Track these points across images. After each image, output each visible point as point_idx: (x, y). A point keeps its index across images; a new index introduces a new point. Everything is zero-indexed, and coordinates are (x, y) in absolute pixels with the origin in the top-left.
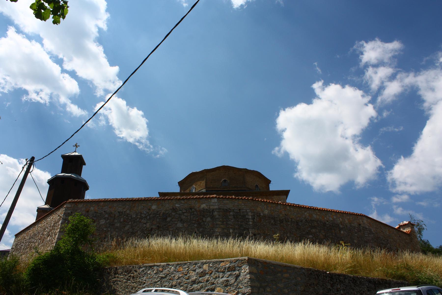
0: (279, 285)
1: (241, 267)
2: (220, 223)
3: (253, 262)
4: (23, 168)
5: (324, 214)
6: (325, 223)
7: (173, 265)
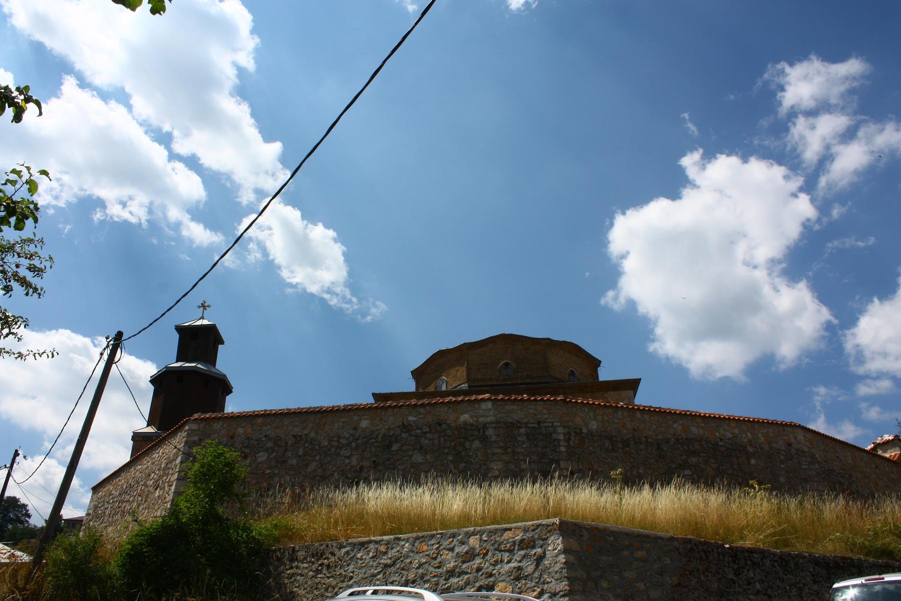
0: (627, 574)
1: (547, 539)
2: (499, 451)
3: (570, 529)
4: (102, 354)
5: (714, 425)
6: (717, 444)
7: (407, 540)
